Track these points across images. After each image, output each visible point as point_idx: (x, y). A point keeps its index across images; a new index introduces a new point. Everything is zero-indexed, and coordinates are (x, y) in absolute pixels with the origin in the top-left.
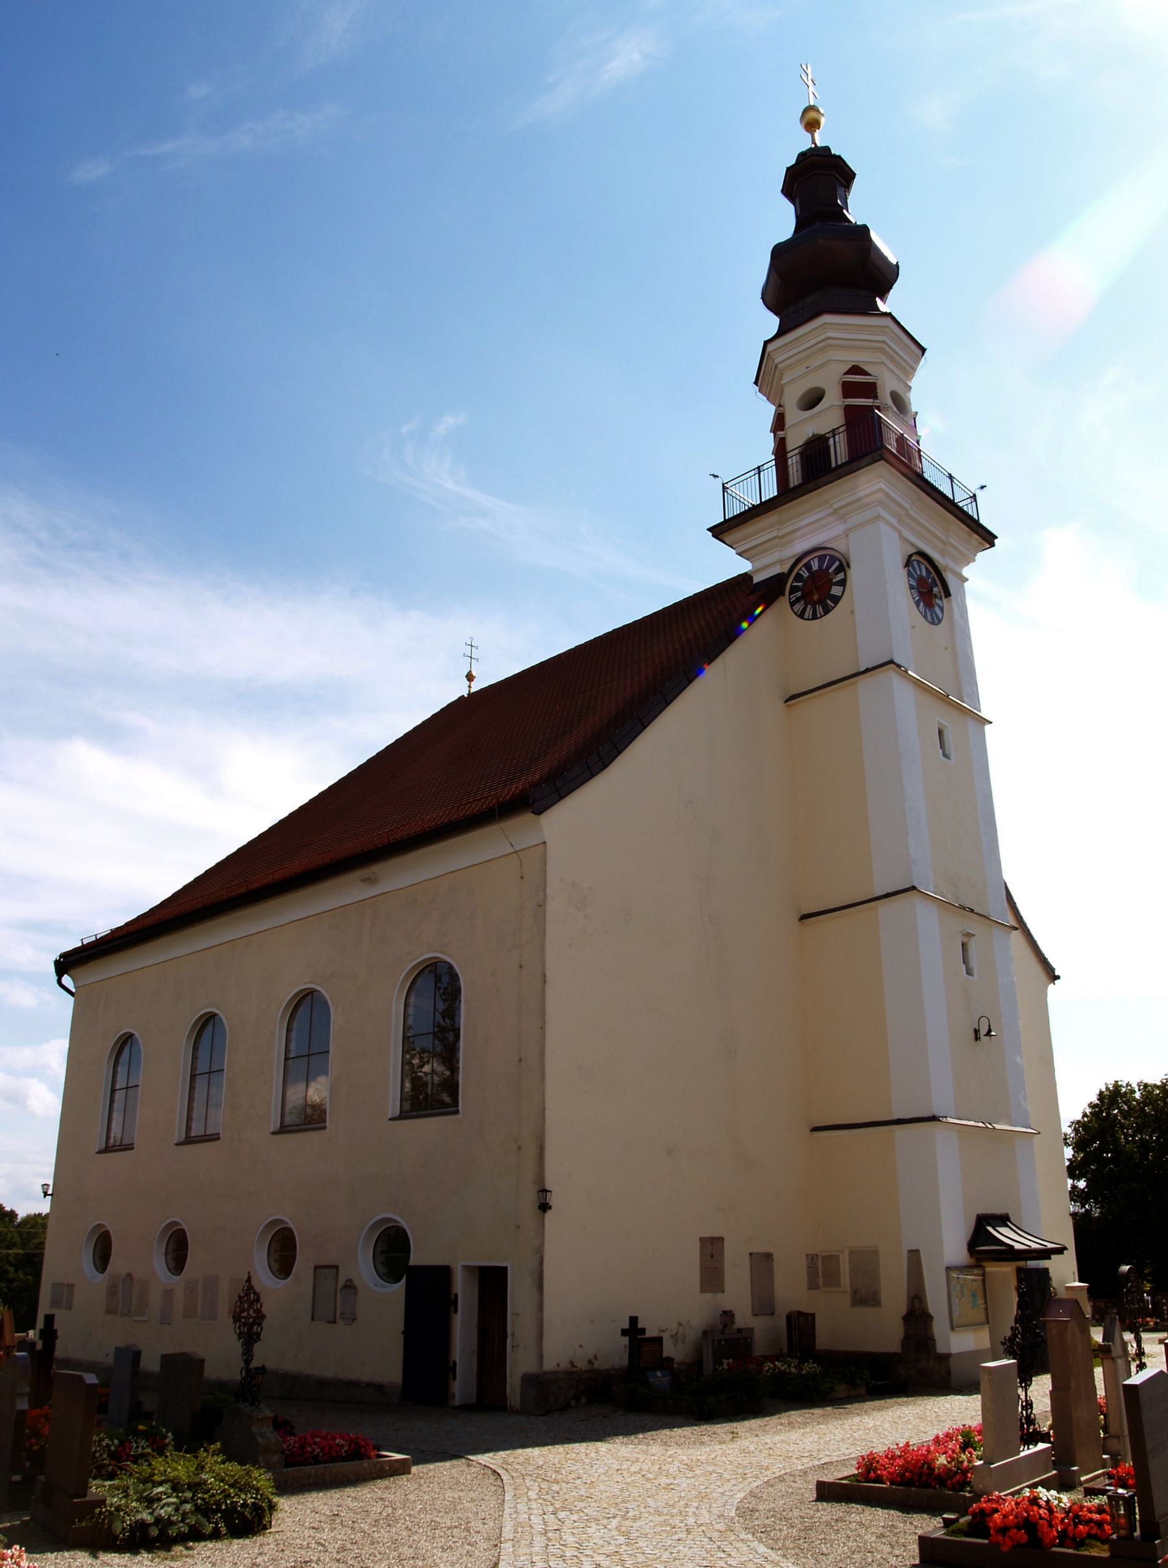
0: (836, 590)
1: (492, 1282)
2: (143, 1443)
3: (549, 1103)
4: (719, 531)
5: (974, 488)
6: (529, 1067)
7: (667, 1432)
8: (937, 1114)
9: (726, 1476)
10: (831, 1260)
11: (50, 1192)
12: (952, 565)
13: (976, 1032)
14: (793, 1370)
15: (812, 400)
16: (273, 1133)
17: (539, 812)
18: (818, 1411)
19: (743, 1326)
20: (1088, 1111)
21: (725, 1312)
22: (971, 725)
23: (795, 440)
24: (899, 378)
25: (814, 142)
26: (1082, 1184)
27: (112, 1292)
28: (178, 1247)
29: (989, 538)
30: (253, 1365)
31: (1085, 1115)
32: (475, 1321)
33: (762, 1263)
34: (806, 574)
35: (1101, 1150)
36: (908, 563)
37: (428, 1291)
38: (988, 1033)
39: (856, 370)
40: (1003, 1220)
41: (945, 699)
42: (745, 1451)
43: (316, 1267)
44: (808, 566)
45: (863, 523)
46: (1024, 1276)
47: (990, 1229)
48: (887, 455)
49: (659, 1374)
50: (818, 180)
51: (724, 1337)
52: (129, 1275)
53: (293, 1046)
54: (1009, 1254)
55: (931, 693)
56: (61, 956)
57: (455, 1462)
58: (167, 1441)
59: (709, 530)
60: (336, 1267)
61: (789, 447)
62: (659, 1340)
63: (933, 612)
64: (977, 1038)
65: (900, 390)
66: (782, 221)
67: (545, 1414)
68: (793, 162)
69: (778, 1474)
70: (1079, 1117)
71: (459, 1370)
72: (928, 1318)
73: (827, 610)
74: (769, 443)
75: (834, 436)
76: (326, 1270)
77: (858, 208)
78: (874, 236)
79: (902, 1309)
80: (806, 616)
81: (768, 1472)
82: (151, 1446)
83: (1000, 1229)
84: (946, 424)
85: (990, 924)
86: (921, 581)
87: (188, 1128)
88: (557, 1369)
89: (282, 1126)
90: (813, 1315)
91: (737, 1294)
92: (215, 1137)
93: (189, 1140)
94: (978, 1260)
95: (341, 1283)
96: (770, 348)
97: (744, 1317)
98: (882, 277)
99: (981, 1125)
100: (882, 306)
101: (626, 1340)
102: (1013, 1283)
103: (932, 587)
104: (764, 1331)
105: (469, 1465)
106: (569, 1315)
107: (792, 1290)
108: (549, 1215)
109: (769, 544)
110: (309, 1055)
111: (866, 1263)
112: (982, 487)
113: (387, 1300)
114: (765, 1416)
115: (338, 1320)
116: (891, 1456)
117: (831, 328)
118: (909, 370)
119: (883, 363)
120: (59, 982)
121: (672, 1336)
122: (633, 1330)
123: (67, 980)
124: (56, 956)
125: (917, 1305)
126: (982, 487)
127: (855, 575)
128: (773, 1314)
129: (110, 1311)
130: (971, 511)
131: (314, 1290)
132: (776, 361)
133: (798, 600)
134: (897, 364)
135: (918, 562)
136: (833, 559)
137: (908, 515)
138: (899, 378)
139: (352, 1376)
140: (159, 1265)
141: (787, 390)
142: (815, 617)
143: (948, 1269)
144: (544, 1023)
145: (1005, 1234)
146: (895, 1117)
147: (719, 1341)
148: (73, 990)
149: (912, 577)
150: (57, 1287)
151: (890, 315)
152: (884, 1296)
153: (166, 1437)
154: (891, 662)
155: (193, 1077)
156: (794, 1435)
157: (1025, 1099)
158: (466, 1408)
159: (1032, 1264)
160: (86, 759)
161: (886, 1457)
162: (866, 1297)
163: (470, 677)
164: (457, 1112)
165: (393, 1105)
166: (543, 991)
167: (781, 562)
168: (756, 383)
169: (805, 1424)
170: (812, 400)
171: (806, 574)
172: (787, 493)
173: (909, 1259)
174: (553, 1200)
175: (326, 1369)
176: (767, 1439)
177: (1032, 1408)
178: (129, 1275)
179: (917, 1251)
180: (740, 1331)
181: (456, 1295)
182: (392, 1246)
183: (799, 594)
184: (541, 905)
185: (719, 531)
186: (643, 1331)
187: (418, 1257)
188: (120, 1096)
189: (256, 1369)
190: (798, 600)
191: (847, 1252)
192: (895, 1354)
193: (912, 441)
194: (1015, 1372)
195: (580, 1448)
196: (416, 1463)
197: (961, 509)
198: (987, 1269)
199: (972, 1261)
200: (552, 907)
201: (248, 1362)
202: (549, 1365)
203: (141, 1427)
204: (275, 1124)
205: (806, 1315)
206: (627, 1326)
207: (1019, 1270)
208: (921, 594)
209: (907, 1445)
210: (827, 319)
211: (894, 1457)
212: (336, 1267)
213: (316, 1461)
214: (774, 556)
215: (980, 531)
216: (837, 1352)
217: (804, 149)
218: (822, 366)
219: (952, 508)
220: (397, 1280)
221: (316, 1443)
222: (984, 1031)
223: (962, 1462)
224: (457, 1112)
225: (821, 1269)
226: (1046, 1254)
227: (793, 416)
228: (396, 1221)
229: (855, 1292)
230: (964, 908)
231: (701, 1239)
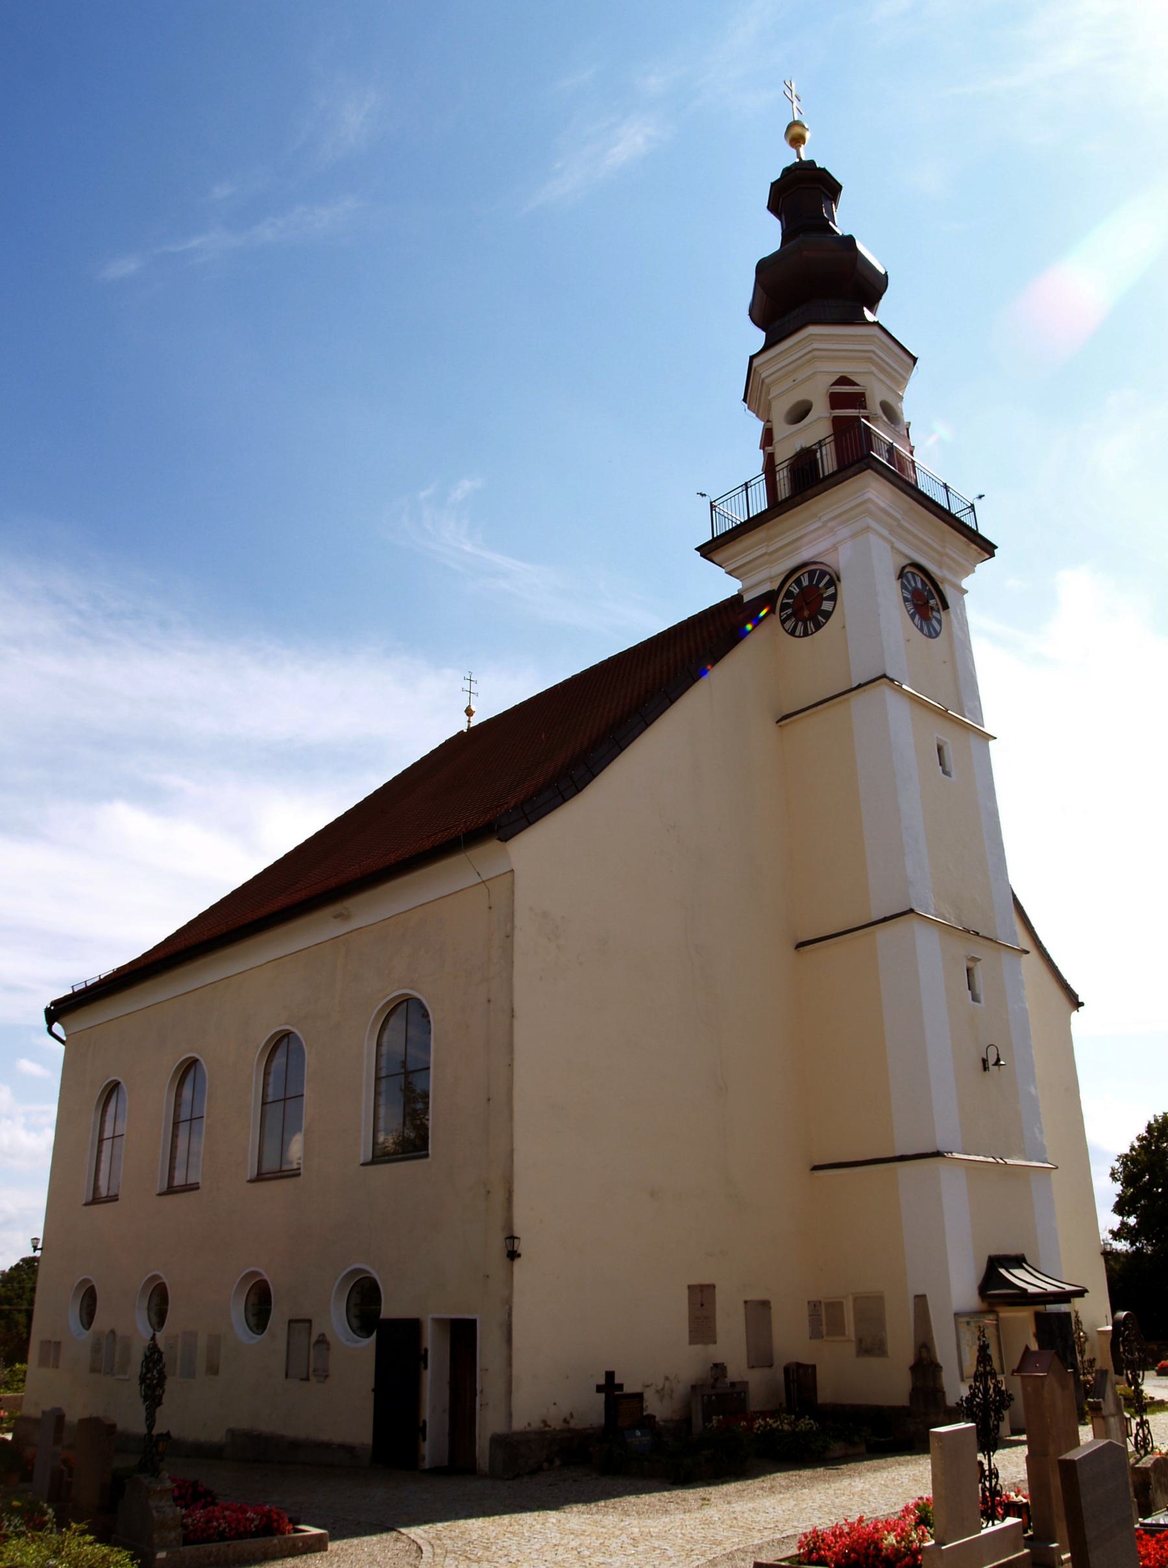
0: (827, 606)
1: (462, 1334)
2: (16, 1521)
3: (517, 1144)
4: (707, 551)
5: (971, 498)
6: (498, 1104)
7: (632, 1499)
8: (941, 1149)
9: (670, 1553)
10: (835, 1307)
11: (40, 1246)
12: (949, 576)
13: (984, 1061)
14: (786, 1427)
15: (800, 413)
16: (250, 1181)
17: (505, 839)
18: (807, 1473)
19: (736, 1379)
20: (1136, 1144)
21: (716, 1365)
22: (974, 741)
23: (784, 452)
24: (889, 388)
25: (799, 156)
26: (1132, 1221)
27: (96, 1348)
29: (988, 549)
30: (155, 1432)
31: (1133, 1148)
32: (447, 1378)
33: (759, 1312)
34: (796, 590)
35: (1152, 1183)
36: (901, 575)
37: (398, 1345)
38: (997, 1063)
39: (843, 381)
40: (1018, 1261)
41: (943, 714)
42: (708, 1523)
43: (291, 1321)
44: (798, 582)
45: (854, 537)
46: (1041, 1320)
47: (1002, 1271)
48: (874, 464)
49: (638, 1433)
50: (804, 195)
51: (717, 1394)
52: (113, 1332)
53: (270, 1090)
54: (1022, 1298)
55: (934, 711)
56: (52, 1004)
57: (384, 1536)
58: (46, 1518)
59: (697, 549)
60: (310, 1321)
61: (778, 461)
62: (639, 1397)
63: (930, 625)
64: (985, 1068)
65: (890, 400)
66: (768, 236)
67: (513, 1479)
68: (779, 177)
69: (728, 1551)
70: (1127, 1151)
71: (435, 1428)
72: (937, 1368)
73: (818, 626)
74: (759, 459)
75: (820, 447)
76: (300, 1325)
77: (845, 219)
78: (860, 246)
79: (910, 1359)
80: (797, 633)
81: (719, 1548)
82: (27, 1523)
83: (1016, 1272)
84: (943, 437)
85: (999, 944)
86: (916, 593)
87: (171, 1177)
88: (528, 1429)
89: (259, 1174)
90: (814, 1367)
91: (731, 1346)
92: (194, 1187)
93: (171, 1190)
94: (990, 1304)
95: (314, 1338)
96: (756, 362)
97: (738, 1369)
98: (866, 287)
99: (991, 1160)
100: (869, 316)
101: (602, 1396)
102: (1032, 1329)
103: (928, 599)
104: (759, 1385)
105: (397, 1540)
106: (539, 1375)
107: (791, 1340)
108: (517, 1263)
109: (757, 562)
110: (285, 1100)
111: (871, 1310)
112: (980, 497)
113: (356, 1356)
114: (748, 1479)
115: (311, 1378)
116: (837, 1533)
117: (817, 338)
118: (901, 380)
119: (872, 373)
120: (50, 1031)
121: (657, 1391)
122: (609, 1385)
123: (57, 1028)
124: (47, 1003)
125: (925, 1355)
126: (980, 497)
128: (771, 1366)
129: (94, 1370)
130: (968, 520)
131: (288, 1344)
132: (763, 376)
133: (788, 618)
134: (889, 375)
135: (913, 574)
136: (823, 574)
137: (901, 526)
138: (889, 388)
139: (324, 1437)
141: (774, 404)
142: (806, 634)
143: (956, 1315)
144: (512, 1060)
145: (1020, 1278)
146: (898, 1153)
147: (710, 1396)
148: (64, 1038)
149: (906, 589)
150: (45, 1344)
151: (876, 324)
152: (891, 1346)
153: (46, 1514)
154: (884, 676)
155: (176, 1124)
156: (769, 1502)
157: (1041, 1132)
158: (437, 1472)
160: (127, 821)
161: (834, 1534)
162: (871, 1346)
163: (469, 712)
164: (427, 1156)
166: (511, 1025)
167: (771, 579)
168: (745, 400)
169: (788, 1488)
170: (800, 413)
171: (796, 590)
172: (777, 507)
173: (916, 1304)
174: (522, 1247)
175: (299, 1429)
176: (738, 1507)
177: (997, 1477)
178: (113, 1332)
179: (924, 1297)
180: (733, 1384)
181: (426, 1350)
182: (364, 1296)
183: (790, 611)
184: (509, 936)
185: (707, 551)
186: (620, 1387)
187: (388, 1310)
188: (107, 1145)
189: (161, 1435)
190: (788, 618)
191: (851, 1298)
192: (903, 1407)
193: (905, 452)
194: (974, 1437)
195: (528, 1519)
196: (334, 1537)
197: (958, 520)
198: (1001, 1315)
199: (984, 1306)
200: (519, 937)
201: (150, 1427)
202: (519, 1424)
203: (16, 1503)
204: (252, 1172)
205: (806, 1367)
206: (602, 1381)
207: (1038, 1316)
208: (916, 606)
209: (861, 1520)
210: (812, 330)
211: (841, 1534)
212: (310, 1321)
213: (222, 1537)
214: (763, 574)
215: (979, 541)
216: (843, 1406)
217: (789, 164)
218: (809, 378)
219: (948, 518)
220: (369, 1335)
221: (224, 1517)
222: (992, 1060)
223: (911, 1542)
224: (427, 1156)
225: (823, 1317)
226: (1064, 1297)
227: (781, 430)
228: (368, 1272)
229: (860, 1341)
230: (969, 932)
231: (689, 1287)
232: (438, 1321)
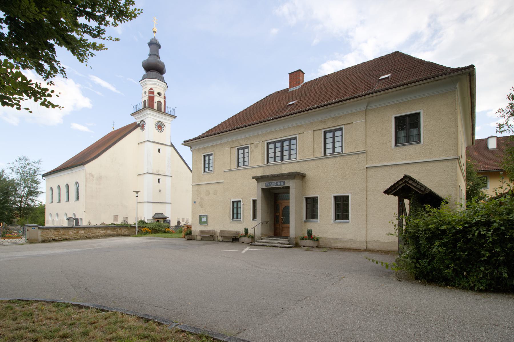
210: (146, 79)
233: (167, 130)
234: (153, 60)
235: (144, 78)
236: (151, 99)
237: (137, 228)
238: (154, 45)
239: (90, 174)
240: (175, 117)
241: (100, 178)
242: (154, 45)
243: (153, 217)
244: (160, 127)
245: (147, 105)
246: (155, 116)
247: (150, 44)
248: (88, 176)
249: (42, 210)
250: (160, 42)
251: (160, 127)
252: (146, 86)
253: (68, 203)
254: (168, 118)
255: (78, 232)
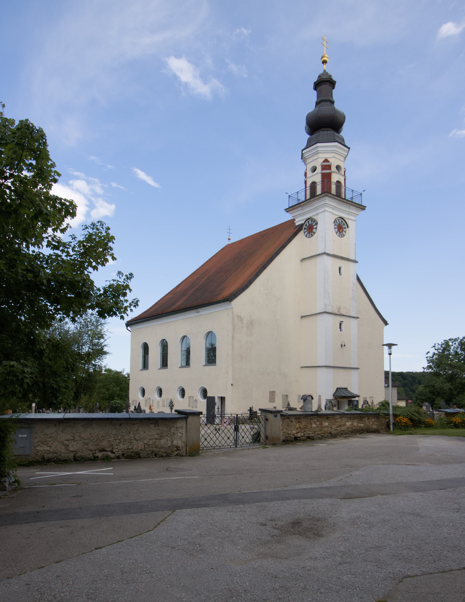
1: (222, 399)
13: (342, 345)
28: (160, 392)
37: (211, 402)
38: (344, 346)
44: (308, 222)
53: (183, 348)
73: (312, 236)
123: (129, 328)
127: (319, 226)
136: (314, 221)
140: (156, 396)
159: (350, 399)
165: (204, 363)
167: (302, 220)
168: (302, 159)
187: (209, 395)
204: (180, 366)
210: (318, 145)
222: (343, 345)
232: (218, 397)
233: (351, 232)
234: (325, 109)
235: (310, 144)
236: (326, 177)
237: (391, 417)
238: (325, 84)
239: (238, 317)
240: (363, 208)
241: (251, 324)
242: (325, 84)
243: (334, 395)
244: (341, 227)
245: (319, 191)
246: (334, 208)
247: (317, 85)
248: (236, 320)
249: (119, 383)
250: (334, 78)
251: (341, 227)
252: (315, 157)
253: (187, 369)
254: (353, 210)
255: (321, 424)
